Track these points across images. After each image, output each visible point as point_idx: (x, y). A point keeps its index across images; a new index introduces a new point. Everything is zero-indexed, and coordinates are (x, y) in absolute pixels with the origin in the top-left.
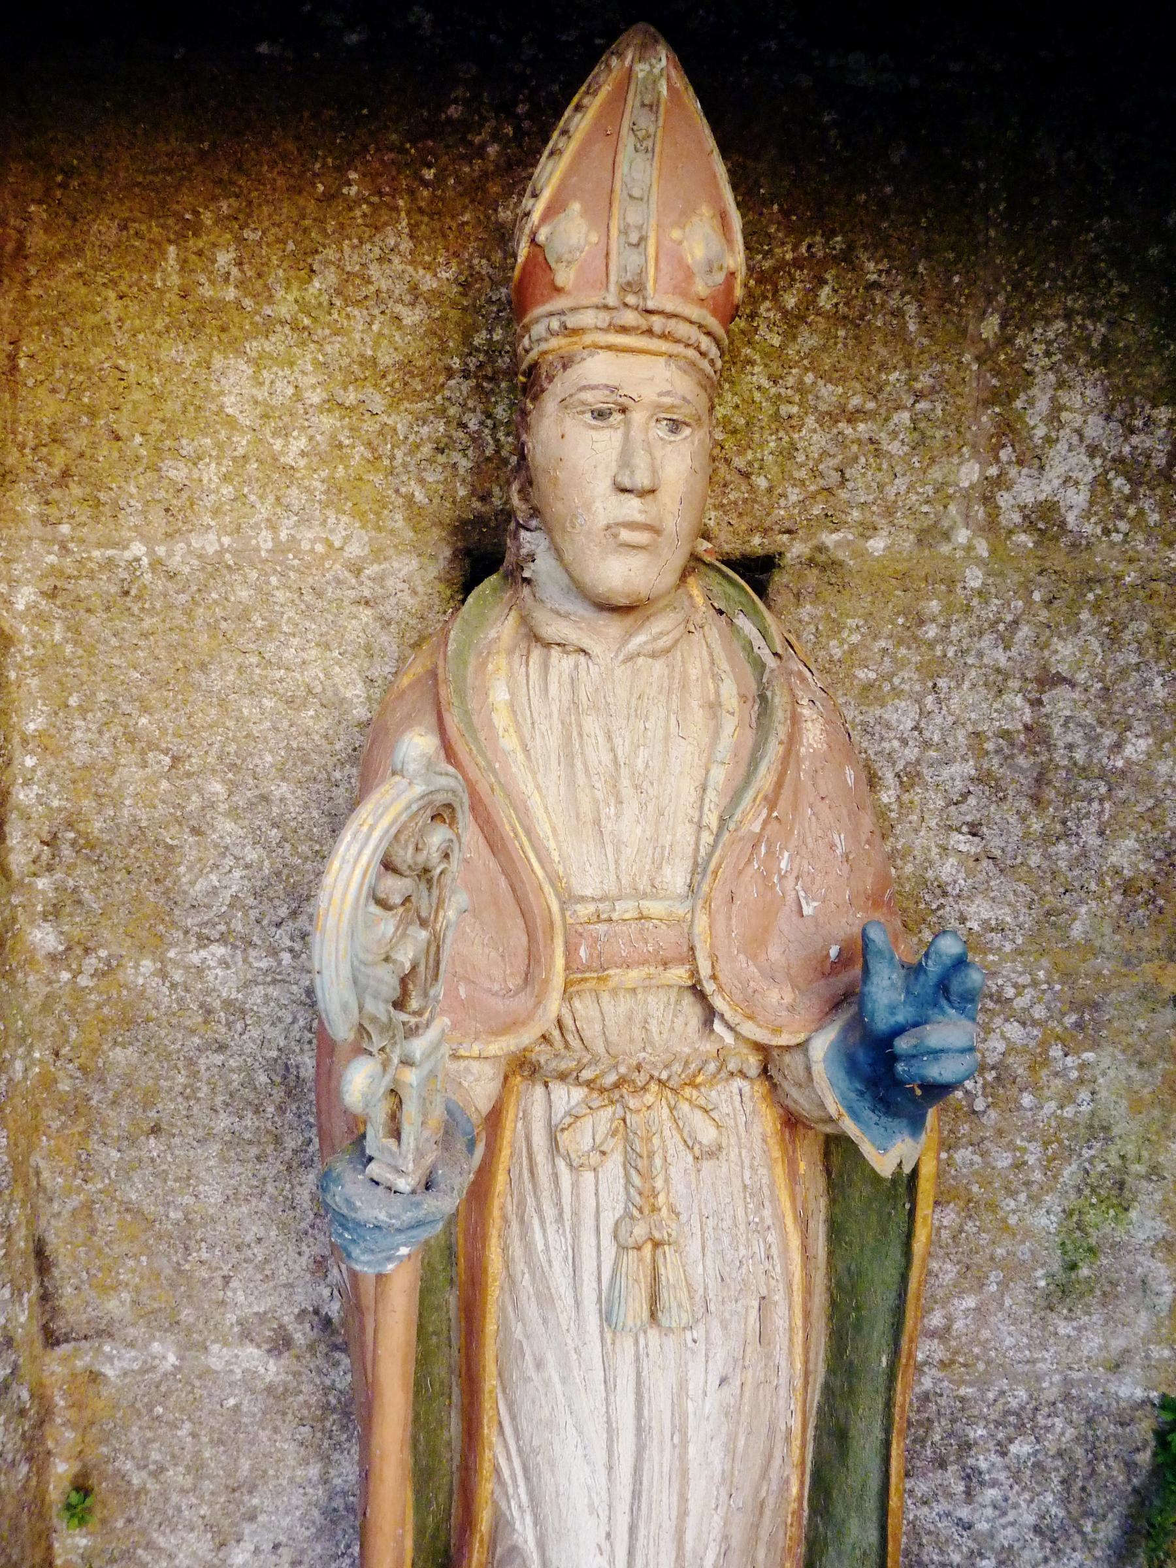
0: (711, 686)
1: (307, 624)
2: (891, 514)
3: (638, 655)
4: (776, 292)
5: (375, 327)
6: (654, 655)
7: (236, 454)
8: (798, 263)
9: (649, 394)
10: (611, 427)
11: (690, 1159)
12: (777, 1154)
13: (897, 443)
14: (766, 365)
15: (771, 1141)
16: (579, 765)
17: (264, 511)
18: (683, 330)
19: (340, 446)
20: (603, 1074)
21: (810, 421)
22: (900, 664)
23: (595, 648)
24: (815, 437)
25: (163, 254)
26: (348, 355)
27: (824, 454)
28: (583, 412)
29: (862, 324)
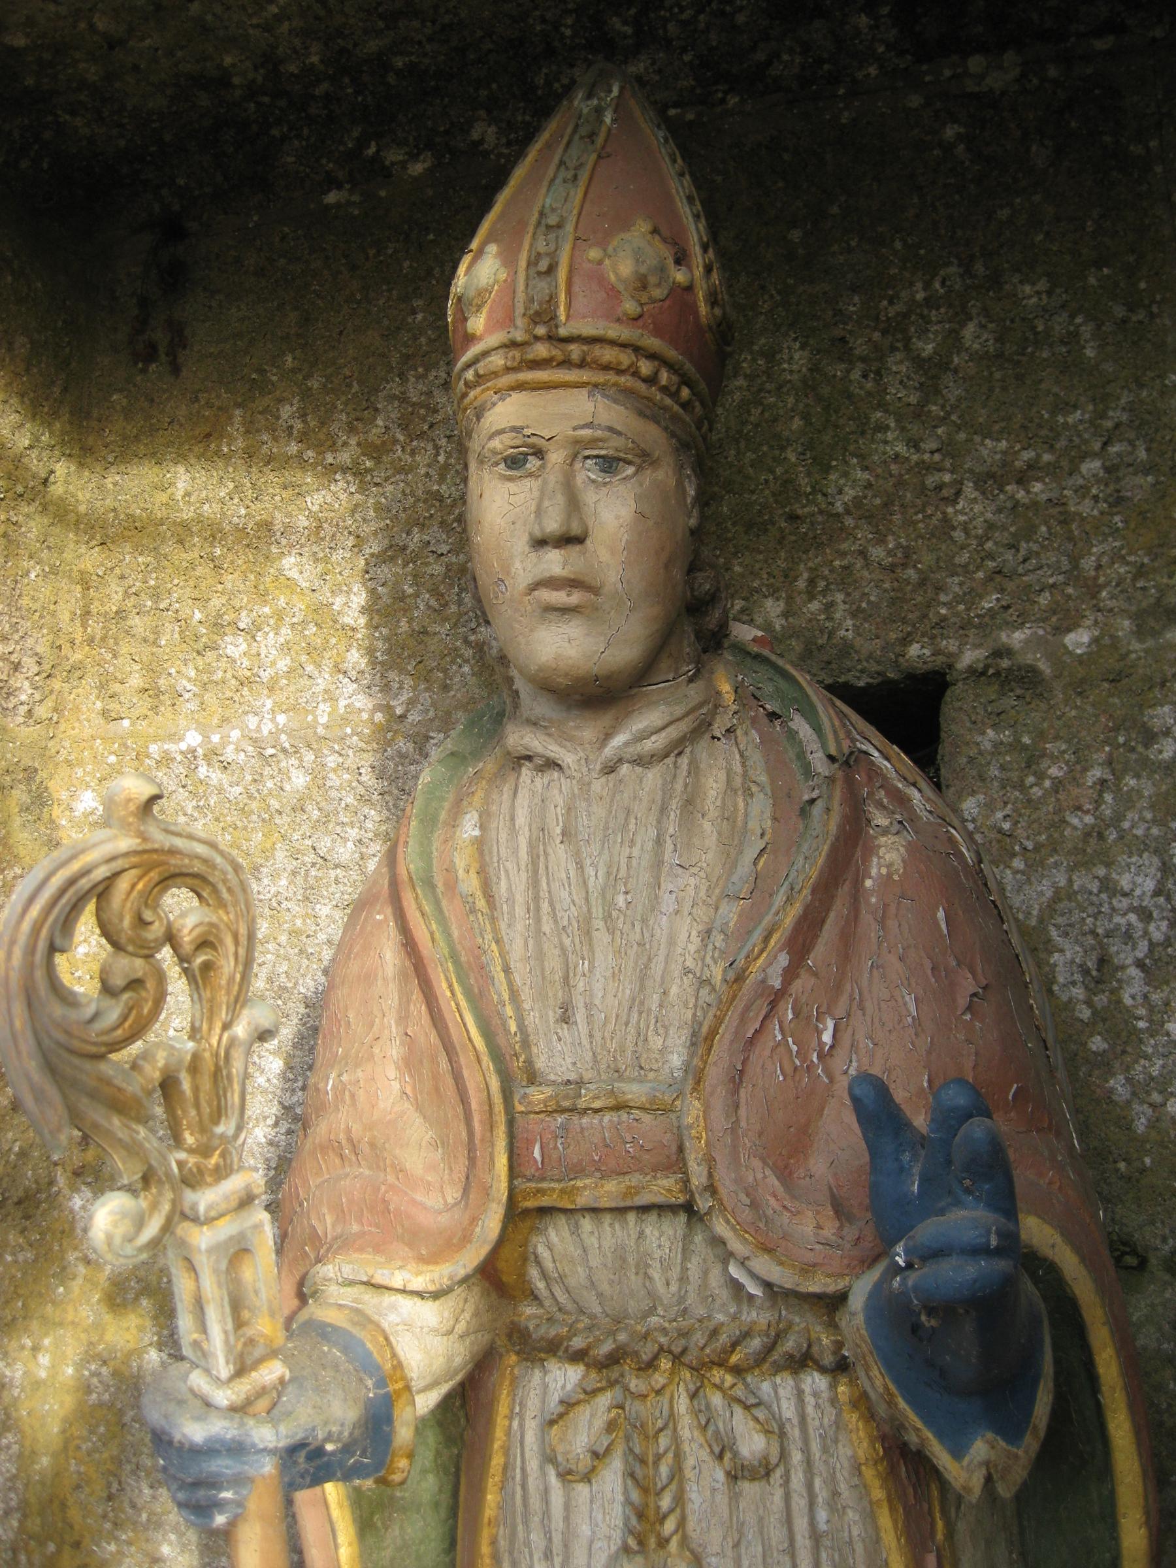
0: (741, 805)
1: (366, 810)
2: (1094, 596)
3: (620, 760)
4: (907, 341)
5: (441, 459)
6: (642, 761)
7: (295, 620)
8: (930, 302)
9: (562, 429)
10: (530, 475)
11: (720, 1475)
12: (878, 1494)
13: (1088, 502)
14: (903, 429)
15: (869, 1473)
16: (545, 907)
17: (323, 682)
18: (608, 354)
19: (403, 598)
20: (598, 1341)
21: (969, 489)
22: (1127, 801)
23: (568, 758)
24: (977, 508)
25: (230, 418)
26: (412, 493)
27: (990, 526)
28: (497, 464)
29: (1024, 359)
